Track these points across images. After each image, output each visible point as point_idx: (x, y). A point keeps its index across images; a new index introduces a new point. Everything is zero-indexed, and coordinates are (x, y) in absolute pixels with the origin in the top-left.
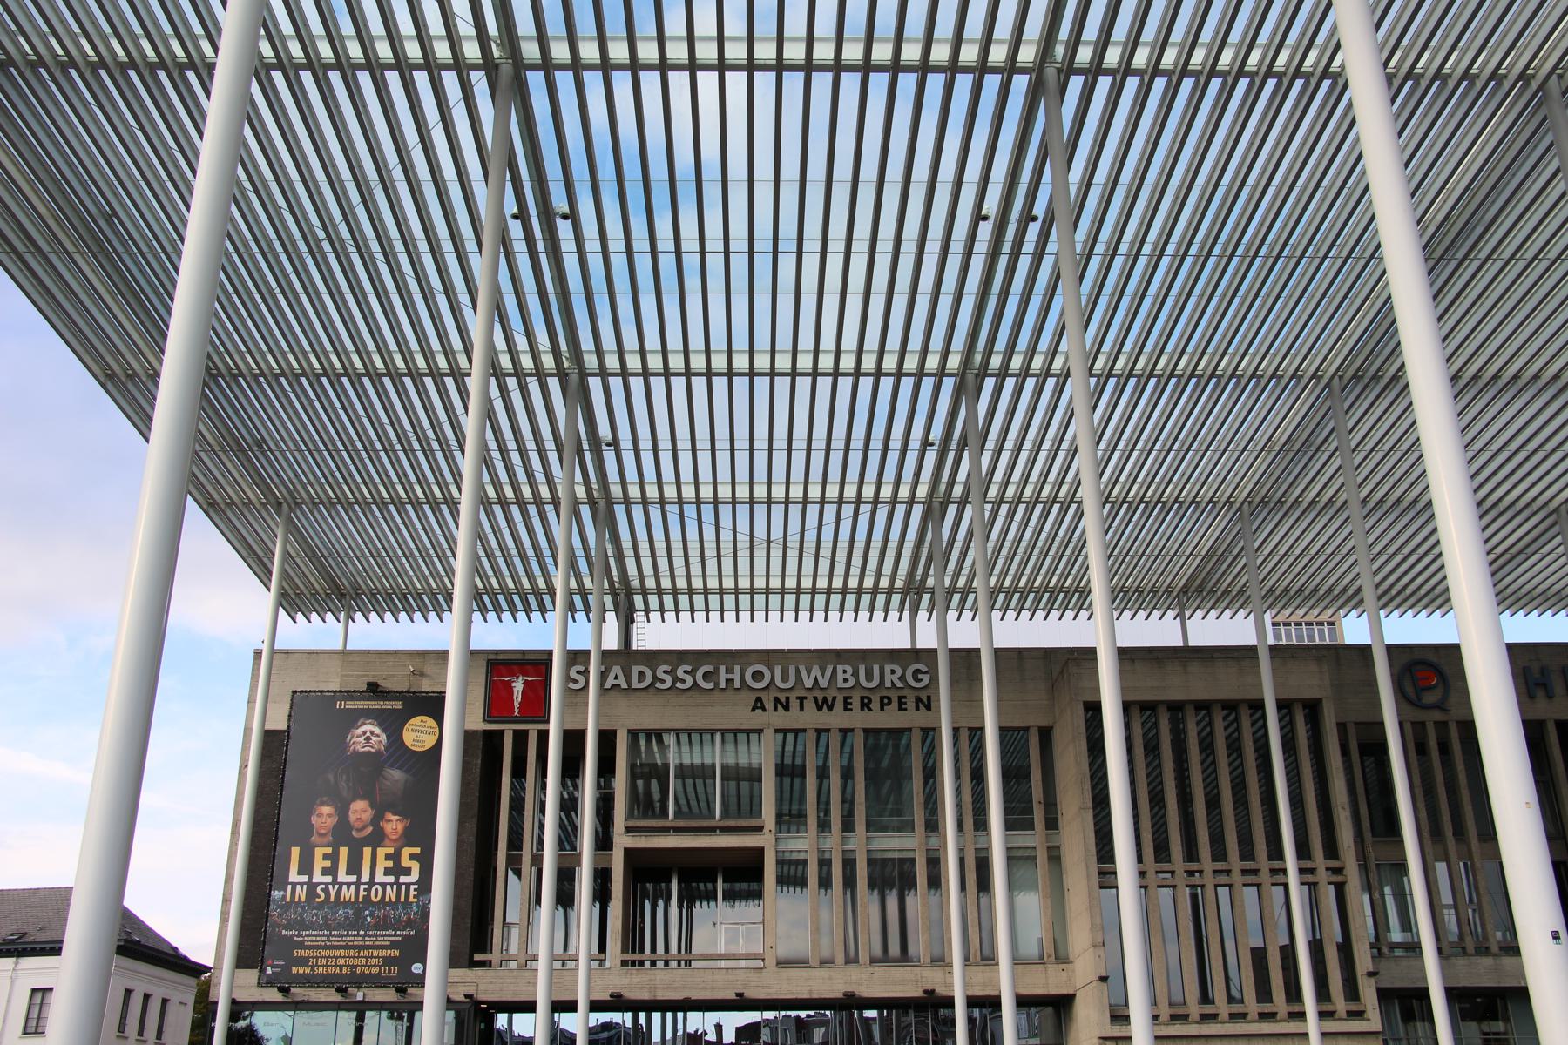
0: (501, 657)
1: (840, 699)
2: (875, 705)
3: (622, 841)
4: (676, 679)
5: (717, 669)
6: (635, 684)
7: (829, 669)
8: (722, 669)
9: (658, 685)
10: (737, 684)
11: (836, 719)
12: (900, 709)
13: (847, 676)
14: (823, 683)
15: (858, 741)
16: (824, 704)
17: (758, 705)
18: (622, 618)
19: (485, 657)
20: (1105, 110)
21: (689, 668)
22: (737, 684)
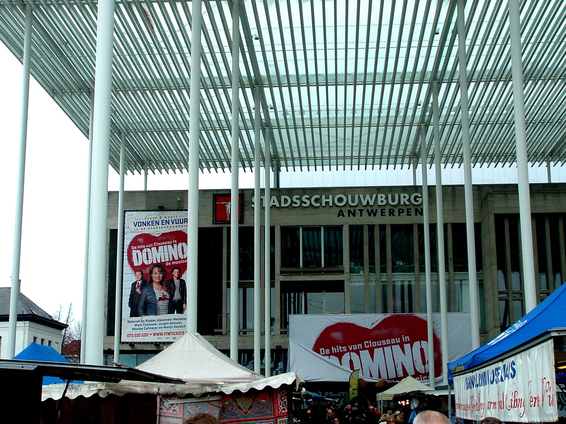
0: (219, 193)
1: (379, 210)
2: (396, 213)
3: (279, 278)
4: (302, 202)
5: (321, 197)
6: (283, 205)
7: (374, 196)
8: (324, 197)
9: (294, 205)
10: (331, 204)
11: (378, 220)
12: (408, 215)
13: (383, 199)
14: (371, 203)
15: (388, 231)
16: (372, 213)
17: (341, 214)
18: (276, 171)
19: (212, 193)
20: (453, 94)
21: (308, 197)
22: (331, 204)
